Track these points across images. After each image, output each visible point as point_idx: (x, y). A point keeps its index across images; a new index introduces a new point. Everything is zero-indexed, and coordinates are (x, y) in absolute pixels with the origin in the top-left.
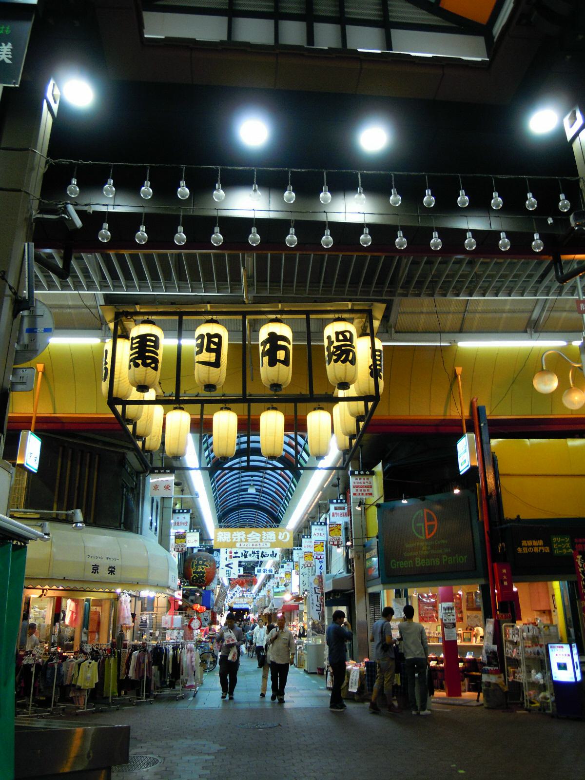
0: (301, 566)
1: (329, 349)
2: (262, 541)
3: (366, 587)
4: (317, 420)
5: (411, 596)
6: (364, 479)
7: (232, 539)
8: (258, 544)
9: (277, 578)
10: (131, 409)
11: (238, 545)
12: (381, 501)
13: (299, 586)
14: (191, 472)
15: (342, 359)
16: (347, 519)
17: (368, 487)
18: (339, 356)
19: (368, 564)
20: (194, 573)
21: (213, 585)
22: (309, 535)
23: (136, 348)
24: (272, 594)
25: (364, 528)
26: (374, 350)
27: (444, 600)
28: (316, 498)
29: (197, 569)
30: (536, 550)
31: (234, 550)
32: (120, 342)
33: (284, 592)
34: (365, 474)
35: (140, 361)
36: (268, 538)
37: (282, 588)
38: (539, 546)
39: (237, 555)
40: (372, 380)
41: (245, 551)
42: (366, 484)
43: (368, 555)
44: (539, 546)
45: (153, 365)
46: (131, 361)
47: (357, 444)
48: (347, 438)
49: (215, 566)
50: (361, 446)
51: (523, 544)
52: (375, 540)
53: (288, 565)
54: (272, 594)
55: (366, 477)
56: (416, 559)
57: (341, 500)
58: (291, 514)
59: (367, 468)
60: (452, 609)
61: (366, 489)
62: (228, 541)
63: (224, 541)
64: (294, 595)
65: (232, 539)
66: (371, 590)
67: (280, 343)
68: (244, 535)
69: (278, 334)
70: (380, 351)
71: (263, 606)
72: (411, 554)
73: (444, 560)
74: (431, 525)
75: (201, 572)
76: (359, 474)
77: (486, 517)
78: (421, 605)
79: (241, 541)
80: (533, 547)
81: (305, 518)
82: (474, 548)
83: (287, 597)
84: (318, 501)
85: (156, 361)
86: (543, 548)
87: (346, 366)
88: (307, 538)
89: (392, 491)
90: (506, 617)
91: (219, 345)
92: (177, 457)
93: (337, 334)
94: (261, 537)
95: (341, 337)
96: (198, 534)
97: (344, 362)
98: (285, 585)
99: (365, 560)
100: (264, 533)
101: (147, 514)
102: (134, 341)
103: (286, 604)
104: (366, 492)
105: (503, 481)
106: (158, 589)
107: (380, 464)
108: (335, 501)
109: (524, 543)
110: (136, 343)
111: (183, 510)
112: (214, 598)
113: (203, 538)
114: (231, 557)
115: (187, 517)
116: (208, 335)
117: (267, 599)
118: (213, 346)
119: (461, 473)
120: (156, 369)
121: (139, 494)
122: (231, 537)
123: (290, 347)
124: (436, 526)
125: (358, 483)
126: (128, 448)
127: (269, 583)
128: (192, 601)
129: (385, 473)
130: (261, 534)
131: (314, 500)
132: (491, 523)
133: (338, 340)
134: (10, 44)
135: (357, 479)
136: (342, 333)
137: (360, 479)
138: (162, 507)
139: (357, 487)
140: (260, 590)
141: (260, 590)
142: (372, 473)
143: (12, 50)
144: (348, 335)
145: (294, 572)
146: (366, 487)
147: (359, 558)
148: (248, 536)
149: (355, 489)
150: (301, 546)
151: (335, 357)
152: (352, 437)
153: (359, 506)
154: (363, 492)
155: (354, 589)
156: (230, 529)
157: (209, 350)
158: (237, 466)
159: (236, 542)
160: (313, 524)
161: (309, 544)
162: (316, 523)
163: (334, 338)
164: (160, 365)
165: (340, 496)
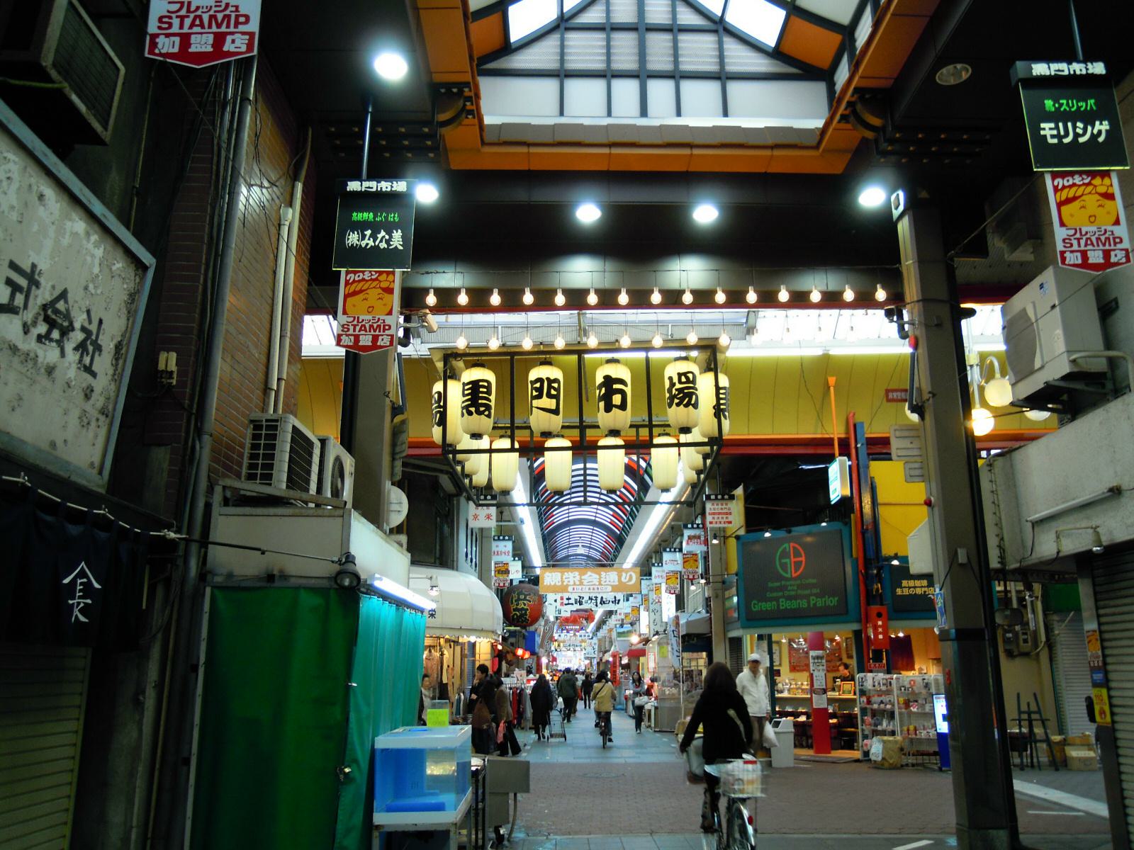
0: (651, 601)
1: (670, 391)
2: (600, 584)
3: (725, 632)
4: (660, 458)
5: (778, 643)
6: (722, 505)
7: (563, 582)
8: (596, 587)
9: (620, 614)
10: (459, 457)
11: (570, 589)
12: (742, 532)
13: (649, 625)
14: (517, 508)
15: (685, 402)
16: (705, 548)
17: (727, 514)
18: (682, 400)
19: (727, 604)
20: (514, 610)
21: (540, 626)
22: (660, 562)
23: (468, 395)
24: (614, 635)
25: (724, 563)
26: (718, 388)
27: (812, 647)
28: (667, 518)
29: (517, 605)
30: (919, 591)
31: (566, 595)
32: (450, 382)
33: (629, 632)
34: (723, 499)
35: (473, 409)
36: (608, 580)
37: (627, 627)
38: (922, 587)
39: (570, 601)
40: (716, 420)
41: (580, 597)
42: (725, 511)
43: (727, 594)
44: (922, 587)
45: (487, 413)
46: (463, 408)
47: (712, 464)
48: (701, 456)
49: (541, 600)
50: (719, 465)
51: (903, 585)
52: (735, 579)
53: (635, 598)
54: (614, 635)
55: (724, 502)
56: (781, 600)
57: (698, 525)
58: (638, 534)
59: (725, 493)
60: (821, 658)
61: (725, 516)
62: (557, 584)
63: (553, 584)
64: (642, 637)
65: (563, 582)
66: (734, 634)
67: (615, 386)
68: (578, 577)
69: (613, 377)
70: (724, 388)
71: (603, 649)
72: (775, 595)
73: (812, 602)
74: (798, 561)
75: (523, 609)
76: (716, 499)
77: (861, 555)
78: (792, 652)
79: (575, 584)
80: (915, 587)
81: (655, 541)
82: (846, 590)
83: (634, 639)
84: (670, 523)
85: (488, 407)
86: (926, 589)
87: (688, 411)
88: (658, 566)
89: (754, 521)
90: (880, 667)
91: (558, 390)
92: (506, 492)
93: (680, 375)
94: (600, 579)
95: (683, 379)
96: (520, 563)
97: (686, 406)
98: (632, 624)
99: (724, 600)
100: (603, 574)
101: (462, 545)
102: (466, 387)
103: (633, 648)
104: (725, 520)
105: (882, 511)
106: (478, 634)
107: (741, 487)
108: (690, 526)
109: (905, 583)
110: (467, 390)
111: (504, 537)
112: (538, 640)
113: (527, 567)
114: (562, 604)
115: (509, 545)
116: (548, 379)
117: (608, 640)
118: (553, 392)
119: (833, 503)
120: (489, 416)
121: (453, 521)
122: (562, 578)
123: (628, 390)
124: (804, 563)
125: (714, 509)
126: (442, 471)
127: (609, 620)
128: (512, 644)
129: (748, 498)
130: (600, 575)
131: (666, 521)
132: (868, 563)
133: (680, 382)
134: (399, 231)
135: (713, 504)
136: (685, 374)
137: (717, 505)
138: (480, 537)
139: (714, 514)
140: (598, 628)
141: (598, 628)
142: (732, 498)
143: (402, 237)
144: (690, 376)
145: (642, 608)
146: (719, 514)
147: (717, 597)
148: (583, 577)
149: (711, 517)
150: (650, 574)
151: (676, 401)
152: (699, 472)
153: (715, 538)
154: (720, 520)
155: (711, 632)
156: (559, 569)
157: (549, 396)
158: (568, 501)
159: (568, 586)
160: (665, 550)
161: (660, 574)
162: (668, 550)
163: (676, 380)
164: (493, 411)
165: (696, 518)
